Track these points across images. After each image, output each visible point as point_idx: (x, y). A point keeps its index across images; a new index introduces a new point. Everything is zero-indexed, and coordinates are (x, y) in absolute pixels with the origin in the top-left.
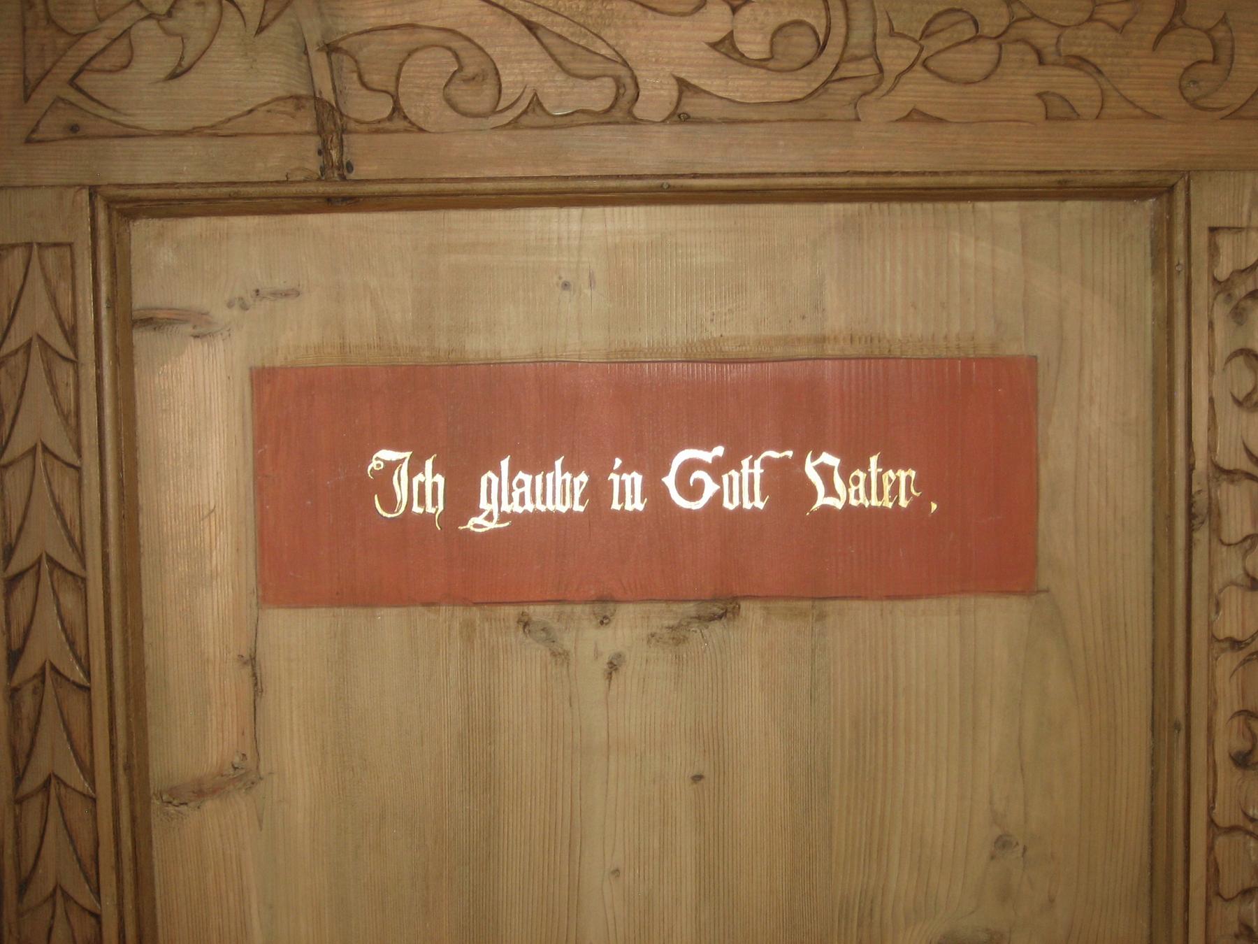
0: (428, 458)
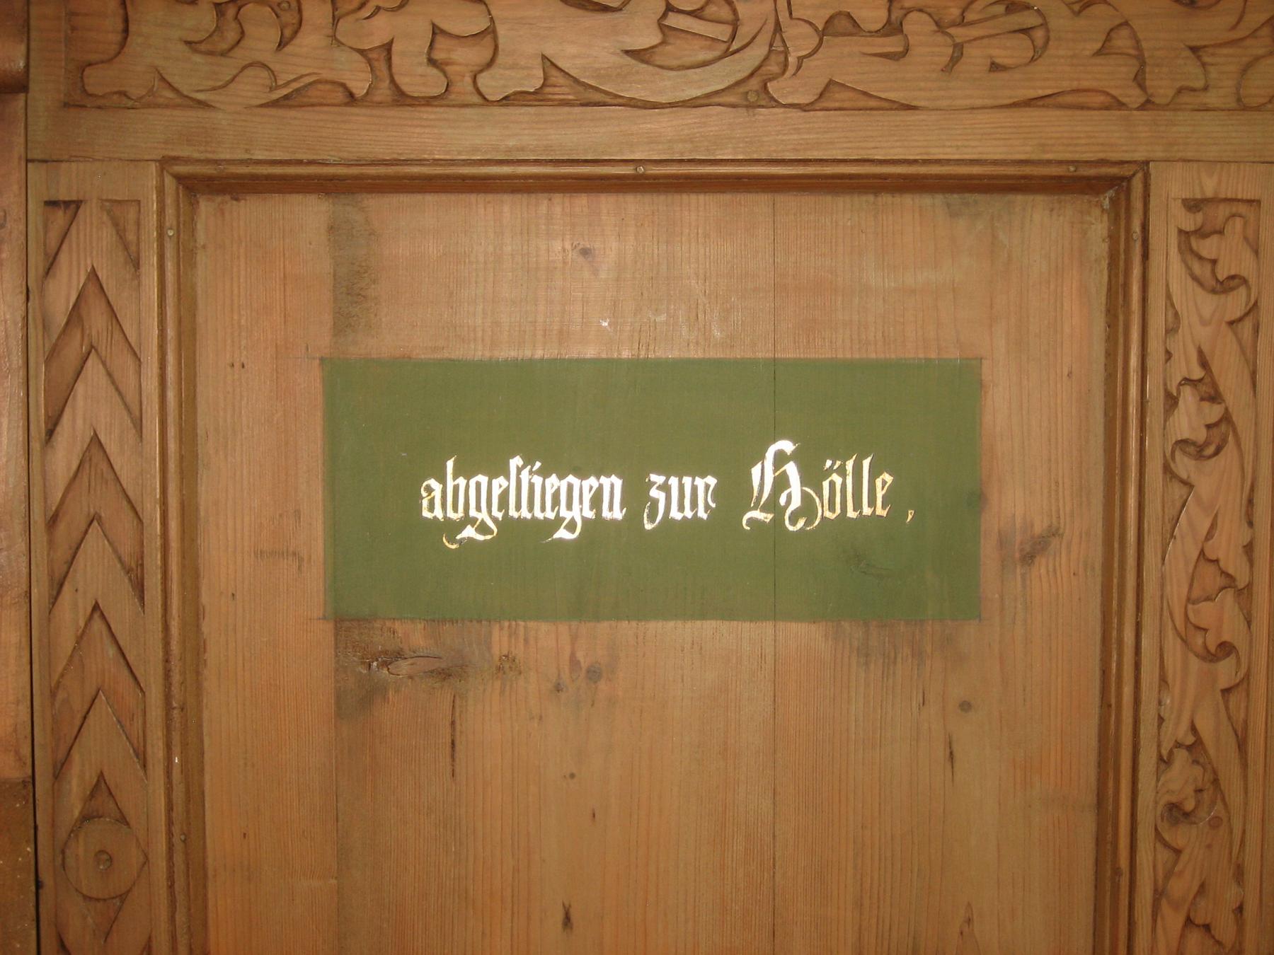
0: (849, 459)
